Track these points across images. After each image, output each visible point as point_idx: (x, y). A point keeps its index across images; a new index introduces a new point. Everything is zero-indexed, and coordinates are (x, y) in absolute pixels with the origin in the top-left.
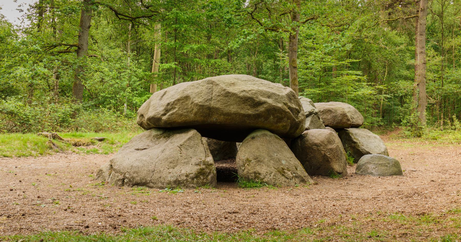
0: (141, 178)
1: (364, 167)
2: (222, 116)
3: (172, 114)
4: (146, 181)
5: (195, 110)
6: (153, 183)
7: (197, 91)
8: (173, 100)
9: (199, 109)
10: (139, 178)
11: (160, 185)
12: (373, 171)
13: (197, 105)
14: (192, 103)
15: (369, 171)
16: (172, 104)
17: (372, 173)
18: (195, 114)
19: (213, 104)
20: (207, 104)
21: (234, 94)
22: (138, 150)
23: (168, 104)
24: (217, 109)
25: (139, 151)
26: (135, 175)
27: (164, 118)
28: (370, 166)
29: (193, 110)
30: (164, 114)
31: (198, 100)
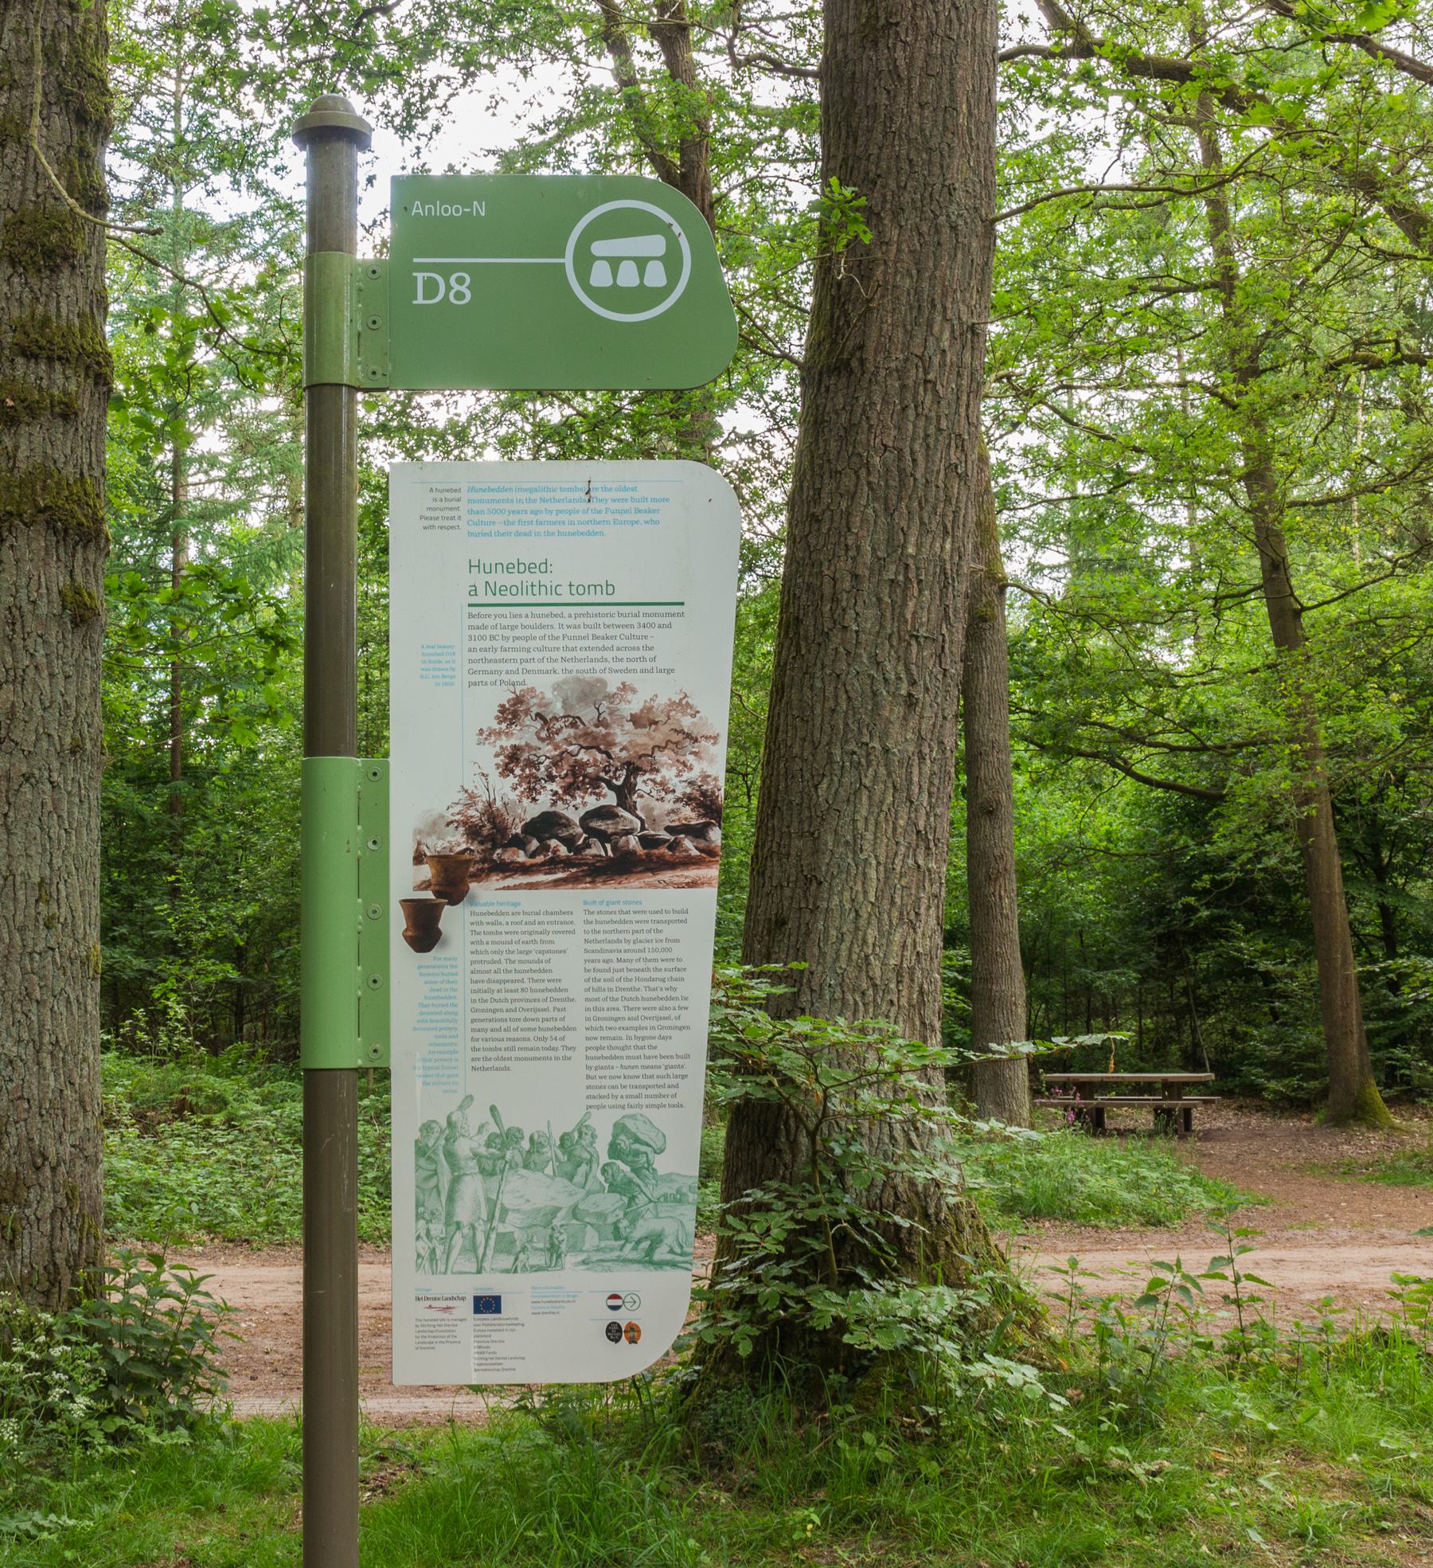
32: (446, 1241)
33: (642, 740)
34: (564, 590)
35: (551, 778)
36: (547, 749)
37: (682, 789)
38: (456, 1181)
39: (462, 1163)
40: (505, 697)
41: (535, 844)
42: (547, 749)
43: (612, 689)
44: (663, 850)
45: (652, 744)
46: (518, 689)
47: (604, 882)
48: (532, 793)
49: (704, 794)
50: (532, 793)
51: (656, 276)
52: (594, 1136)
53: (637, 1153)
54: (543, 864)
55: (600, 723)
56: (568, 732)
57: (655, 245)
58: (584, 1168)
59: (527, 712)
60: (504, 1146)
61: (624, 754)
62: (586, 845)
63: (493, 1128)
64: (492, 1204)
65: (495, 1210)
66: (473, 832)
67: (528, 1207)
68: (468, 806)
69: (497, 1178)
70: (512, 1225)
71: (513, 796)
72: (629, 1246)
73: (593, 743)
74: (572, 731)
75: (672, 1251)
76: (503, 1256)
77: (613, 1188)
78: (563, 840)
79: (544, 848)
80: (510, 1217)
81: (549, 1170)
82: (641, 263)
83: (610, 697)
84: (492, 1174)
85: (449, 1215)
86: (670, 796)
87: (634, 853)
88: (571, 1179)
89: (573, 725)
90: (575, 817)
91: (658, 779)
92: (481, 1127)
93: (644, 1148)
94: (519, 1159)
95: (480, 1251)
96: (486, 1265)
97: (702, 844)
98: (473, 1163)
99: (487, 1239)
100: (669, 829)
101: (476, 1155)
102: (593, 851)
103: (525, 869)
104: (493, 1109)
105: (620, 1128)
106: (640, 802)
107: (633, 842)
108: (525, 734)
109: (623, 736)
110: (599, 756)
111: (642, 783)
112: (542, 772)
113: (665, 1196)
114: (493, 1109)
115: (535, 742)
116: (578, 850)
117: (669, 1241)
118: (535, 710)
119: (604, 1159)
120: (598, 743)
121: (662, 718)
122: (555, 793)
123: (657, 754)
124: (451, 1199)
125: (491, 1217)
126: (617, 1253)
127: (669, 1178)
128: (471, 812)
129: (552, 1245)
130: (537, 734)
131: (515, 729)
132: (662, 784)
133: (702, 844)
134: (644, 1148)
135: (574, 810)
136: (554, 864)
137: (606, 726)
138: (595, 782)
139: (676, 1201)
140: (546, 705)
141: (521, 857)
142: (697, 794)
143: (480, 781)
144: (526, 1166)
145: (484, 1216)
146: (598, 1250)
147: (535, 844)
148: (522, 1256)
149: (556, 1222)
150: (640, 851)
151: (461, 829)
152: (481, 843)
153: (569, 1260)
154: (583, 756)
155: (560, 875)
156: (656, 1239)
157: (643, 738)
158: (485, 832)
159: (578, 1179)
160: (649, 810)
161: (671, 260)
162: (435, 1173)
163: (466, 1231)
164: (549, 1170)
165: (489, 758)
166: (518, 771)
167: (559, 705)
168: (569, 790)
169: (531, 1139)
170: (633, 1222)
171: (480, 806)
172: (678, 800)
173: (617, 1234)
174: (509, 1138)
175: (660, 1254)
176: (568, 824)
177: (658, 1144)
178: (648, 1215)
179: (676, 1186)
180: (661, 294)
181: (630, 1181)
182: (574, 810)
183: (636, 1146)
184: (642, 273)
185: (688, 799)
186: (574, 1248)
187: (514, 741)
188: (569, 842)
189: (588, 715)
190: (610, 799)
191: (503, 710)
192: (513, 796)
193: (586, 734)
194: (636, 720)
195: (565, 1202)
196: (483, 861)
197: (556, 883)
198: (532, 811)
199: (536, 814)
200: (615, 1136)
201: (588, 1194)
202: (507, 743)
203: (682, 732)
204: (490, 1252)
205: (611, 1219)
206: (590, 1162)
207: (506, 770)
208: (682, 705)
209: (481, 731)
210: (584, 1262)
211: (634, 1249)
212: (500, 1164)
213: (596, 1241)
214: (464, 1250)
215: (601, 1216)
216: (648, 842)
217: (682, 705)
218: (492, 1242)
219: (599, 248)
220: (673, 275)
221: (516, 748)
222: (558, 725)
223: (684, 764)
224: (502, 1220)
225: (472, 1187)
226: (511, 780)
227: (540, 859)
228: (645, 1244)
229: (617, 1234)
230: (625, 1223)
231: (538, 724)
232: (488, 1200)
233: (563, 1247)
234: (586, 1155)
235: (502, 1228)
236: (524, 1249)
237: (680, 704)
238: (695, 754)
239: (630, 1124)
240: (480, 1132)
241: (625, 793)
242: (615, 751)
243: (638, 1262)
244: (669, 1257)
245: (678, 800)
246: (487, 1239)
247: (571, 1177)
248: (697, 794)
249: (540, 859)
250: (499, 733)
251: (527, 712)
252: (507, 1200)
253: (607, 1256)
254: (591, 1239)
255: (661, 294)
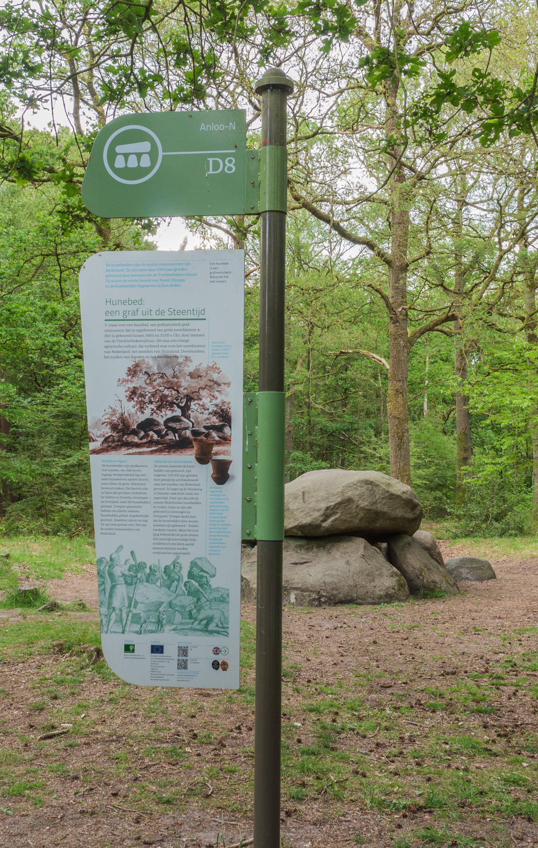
0: (344, 595)
1: (455, 572)
2: (388, 521)
3: (336, 520)
4: (352, 597)
5: (361, 514)
6: (361, 599)
7: (358, 492)
8: (333, 504)
9: (365, 514)
10: (341, 595)
11: (370, 600)
12: (469, 576)
13: (363, 509)
14: (357, 506)
15: (463, 576)
16: (333, 509)
17: (468, 579)
18: (361, 520)
19: (379, 507)
20: (374, 507)
21: (398, 497)
22: (296, 564)
23: (327, 508)
24: (384, 513)
25: (298, 566)
26: (335, 592)
27: (326, 524)
28: (462, 570)
29: (358, 514)
30: (324, 521)
31: (364, 504)
32: (108, 616)
33: (194, 385)
34: (167, 313)
35: (151, 402)
36: (150, 389)
37: (212, 408)
38: (113, 587)
39: (117, 578)
40: (130, 364)
41: (142, 433)
42: (150, 389)
43: (180, 360)
44: (202, 437)
45: (199, 386)
46: (137, 360)
47: (174, 452)
48: (142, 409)
49: (222, 410)
50: (142, 409)
51: (146, 162)
52: (181, 568)
53: (202, 577)
54: (146, 443)
55: (175, 376)
56: (159, 381)
57: (145, 147)
58: (175, 583)
59: (141, 371)
60: (137, 571)
61: (185, 391)
62: (167, 434)
63: (133, 562)
64: (130, 599)
65: (132, 602)
66: (114, 427)
67: (148, 601)
68: (112, 415)
69: (133, 586)
70: (140, 610)
71: (133, 411)
72: (196, 623)
73: (171, 386)
74: (161, 380)
75: (217, 626)
76: (135, 625)
77: (189, 594)
78: (156, 432)
79: (146, 435)
80: (139, 606)
81: (158, 584)
82: (139, 156)
83: (180, 364)
84: (131, 584)
85: (110, 604)
86: (206, 412)
87: (189, 438)
88: (169, 589)
89: (162, 377)
90: (161, 421)
91: (201, 403)
92: (126, 561)
93: (205, 574)
94: (144, 577)
95: (124, 622)
96: (127, 629)
97: (221, 434)
98: (122, 579)
99: (128, 616)
100: (205, 427)
101: (124, 575)
102: (169, 437)
103: (138, 445)
104: (132, 553)
105: (194, 564)
106: (192, 414)
107: (188, 433)
108: (140, 381)
109: (186, 383)
110: (174, 392)
111: (193, 405)
112: (147, 400)
113: (215, 598)
114: (132, 553)
115: (144, 385)
116: (162, 437)
117: (216, 621)
118: (144, 370)
119: (185, 579)
120: (173, 386)
121: (204, 374)
122: (153, 410)
123: (201, 391)
124: (111, 596)
125: (130, 606)
126: (190, 626)
127: (217, 590)
128: (114, 418)
129: (159, 620)
130: (145, 381)
131: (135, 379)
132: (203, 406)
133: (221, 434)
134: (205, 574)
135: (161, 418)
136: (151, 443)
137: (177, 378)
138: (171, 404)
139: (220, 601)
140: (150, 368)
141: (136, 440)
142: (219, 411)
143: (118, 403)
144: (147, 581)
145: (126, 605)
146: (181, 624)
147: (142, 433)
148: (144, 625)
149: (161, 609)
150: (191, 437)
151: (109, 426)
152: (118, 433)
153: (167, 628)
154: (166, 392)
155: (154, 448)
156: (210, 620)
157: (195, 384)
158: (120, 427)
159: (173, 588)
160: (196, 418)
161: (153, 154)
162: (103, 583)
163: (117, 612)
164: (158, 584)
165: (123, 392)
166: (136, 399)
167: (156, 368)
168: (159, 408)
169: (150, 568)
170: (199, 611)
171: (118, 415)
172: (210, 414)
173: (191, 616)
174: (140, 567)
175: (212, 627)
176: (158, 424)
177: (212, 573)
178: (206, 608)
179: (220, 594)
180: (148, 170)
181: (198, 591)
182: (161, 418)
183: (201, 573)
184: (139, 161)
185: (215, 413)
186: (170, 622)
187: (134, 385)
188: (158, 433)
189: (169, 372)
190: (178, 412)
191: (129, 370)
192: (133, 411)
193: (168, 382)
194: (191, 375)
195: (166, 599)
196: (119, 441)
197: (152, 452)
198: (142, 418)
199: (143, 419)
200: (191, 568)
201: (177, 596)
202: (131, 385)
203: (213, 381)
204: (129, 623)
205: (188, 609)
206: (178, 580)
207: (130, 398)
208: (214, 368)
209: (119, 380)
210: (174, 630)
211: (199, 624)
212: (135, 580)
213: (180, 620)
214: (116, 621)
215: (183, 607)
216: (196, 433)
217: (214, 368)
218: (130, 618)
219: (119, 149)
220: (154, 161)
221: (135, 388)
222: (155, 377)
223: (214, 396)
224: (135, 607)
225: (121, 590)
226: (133, 403)
227: (145, 440)
228: (204, 622)
229: (191, 616)
230: (195, 611)
231: (146, 377)
232: (129, 597)
233: (164, 621)
234: (177, 577)
235: (135, 611)
236: (145, 622)
237: (212, 367)
238: (219, 391)
239: (199, 562)
240: (125, 563)
241: (185, 410)
242: (181, 390)
243: (201, 630)
244: (216, 629)
245: (210, 414)
246: (128, 616)
247: (169, 587)
248: (219, 411)
249: (145, 440)
250: (127, 381)
251: (141, 371)
252: (138, 597)
253: (185, 627)
254: (178, 618)
255: (148, 170)
